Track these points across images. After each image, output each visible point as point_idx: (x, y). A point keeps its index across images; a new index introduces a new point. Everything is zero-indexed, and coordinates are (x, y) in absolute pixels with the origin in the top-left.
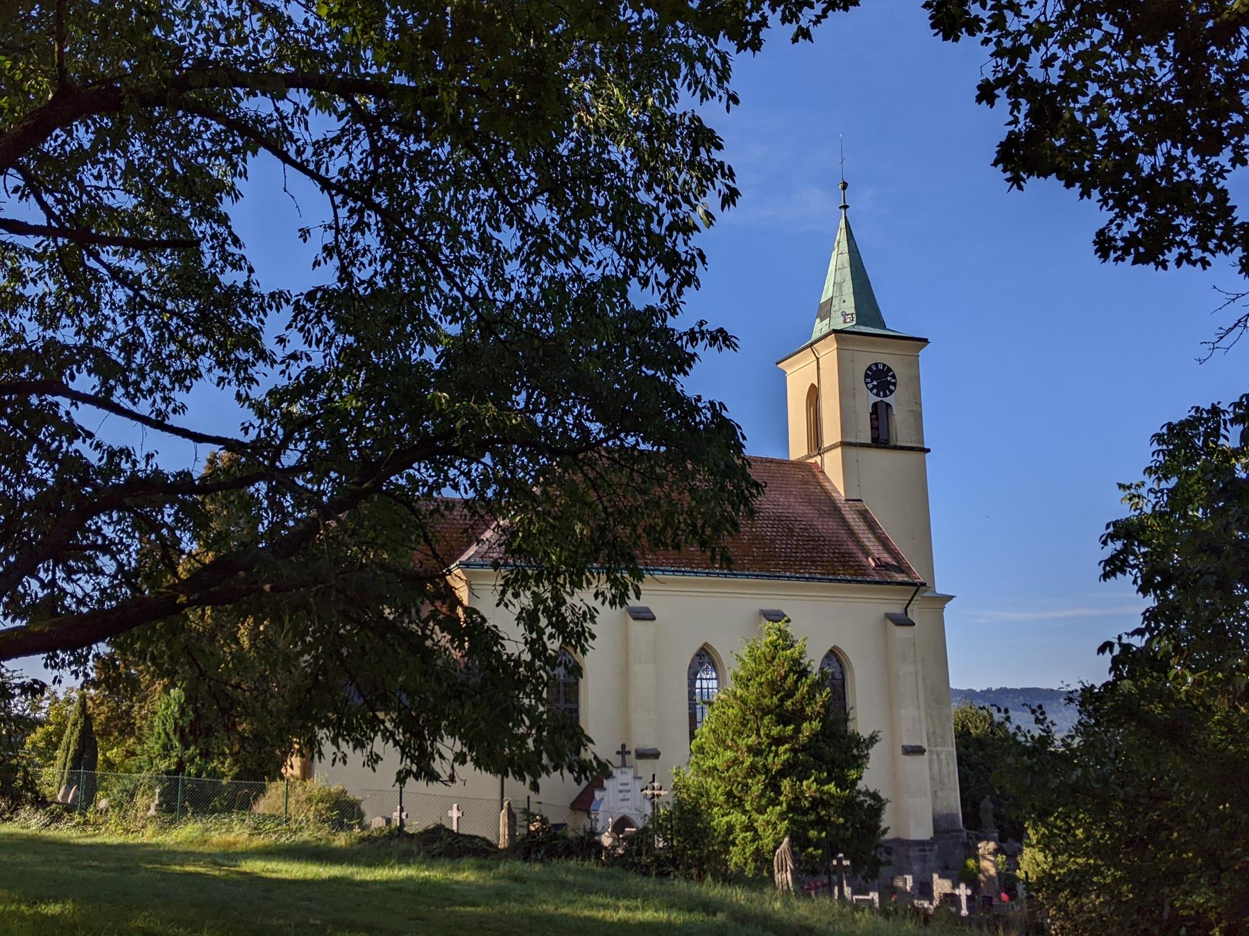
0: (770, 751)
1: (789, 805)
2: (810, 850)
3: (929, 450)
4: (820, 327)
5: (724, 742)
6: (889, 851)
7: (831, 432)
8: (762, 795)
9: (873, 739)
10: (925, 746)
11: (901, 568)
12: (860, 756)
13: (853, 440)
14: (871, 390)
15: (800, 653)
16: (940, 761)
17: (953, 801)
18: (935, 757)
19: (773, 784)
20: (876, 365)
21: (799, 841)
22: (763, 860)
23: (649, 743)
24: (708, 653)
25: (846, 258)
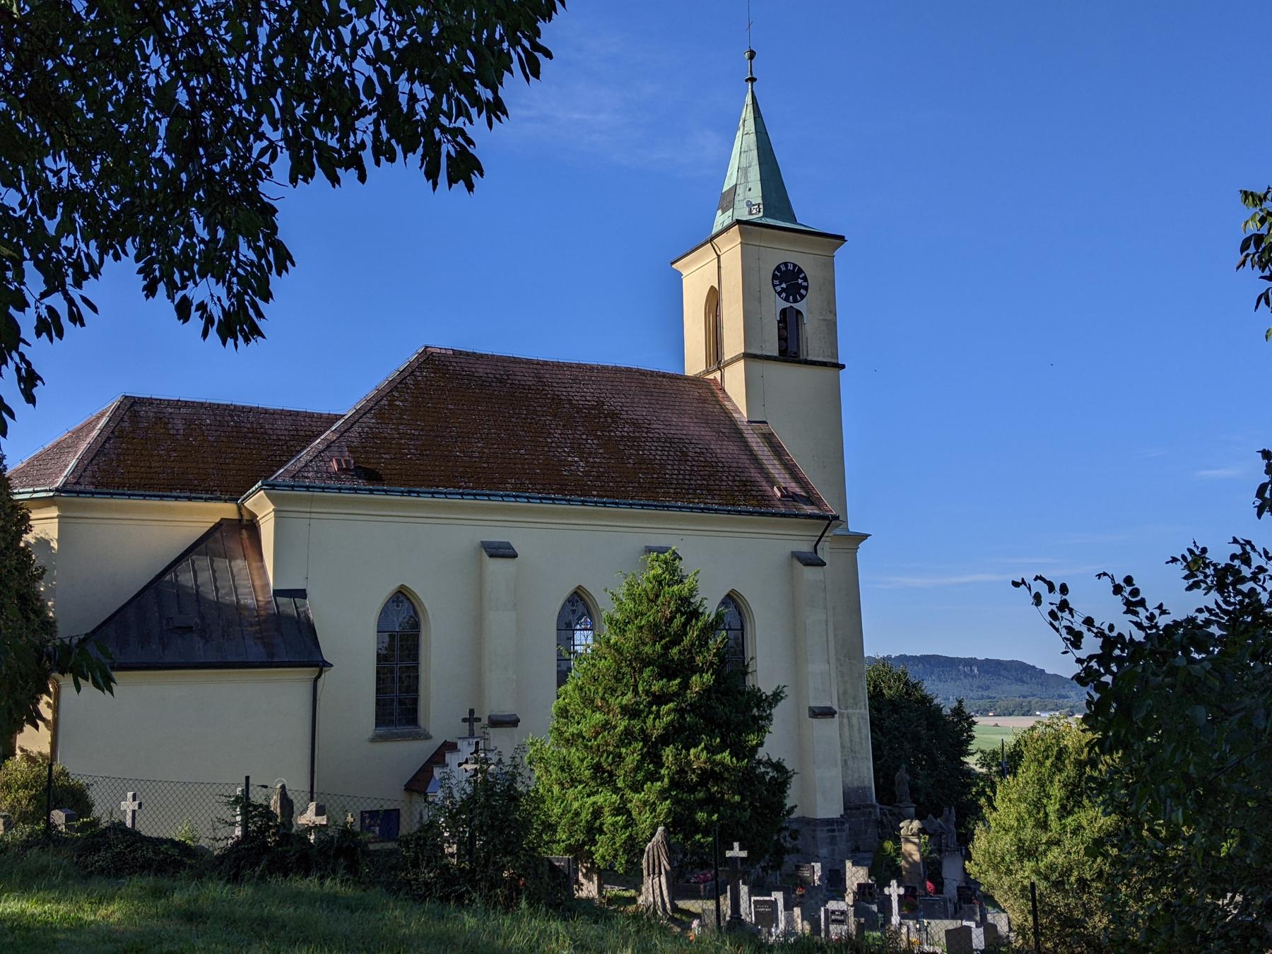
0: (650, 712)
1: (672, 780)
2: (698, 837)
3: (843, 367)
4: (722, 219)
5: (593, 701)
6: (794, 835)
7: (734, 343)
8: (637, 769)
9: (777, 696)
10: (836, 708)
11: (811, 499)
12: (761, 718)
13: (758, 352)
14: (780, 294)
15: (691, 590)
16: (851, 726)
17: (865, 772)
18: (845, 721)
19: (653, 755)
20: (786, 264)
21: (679, 824)
22: (634, 849)
23: (505, 708)
24: (582, 599)
25: (752, 138)
